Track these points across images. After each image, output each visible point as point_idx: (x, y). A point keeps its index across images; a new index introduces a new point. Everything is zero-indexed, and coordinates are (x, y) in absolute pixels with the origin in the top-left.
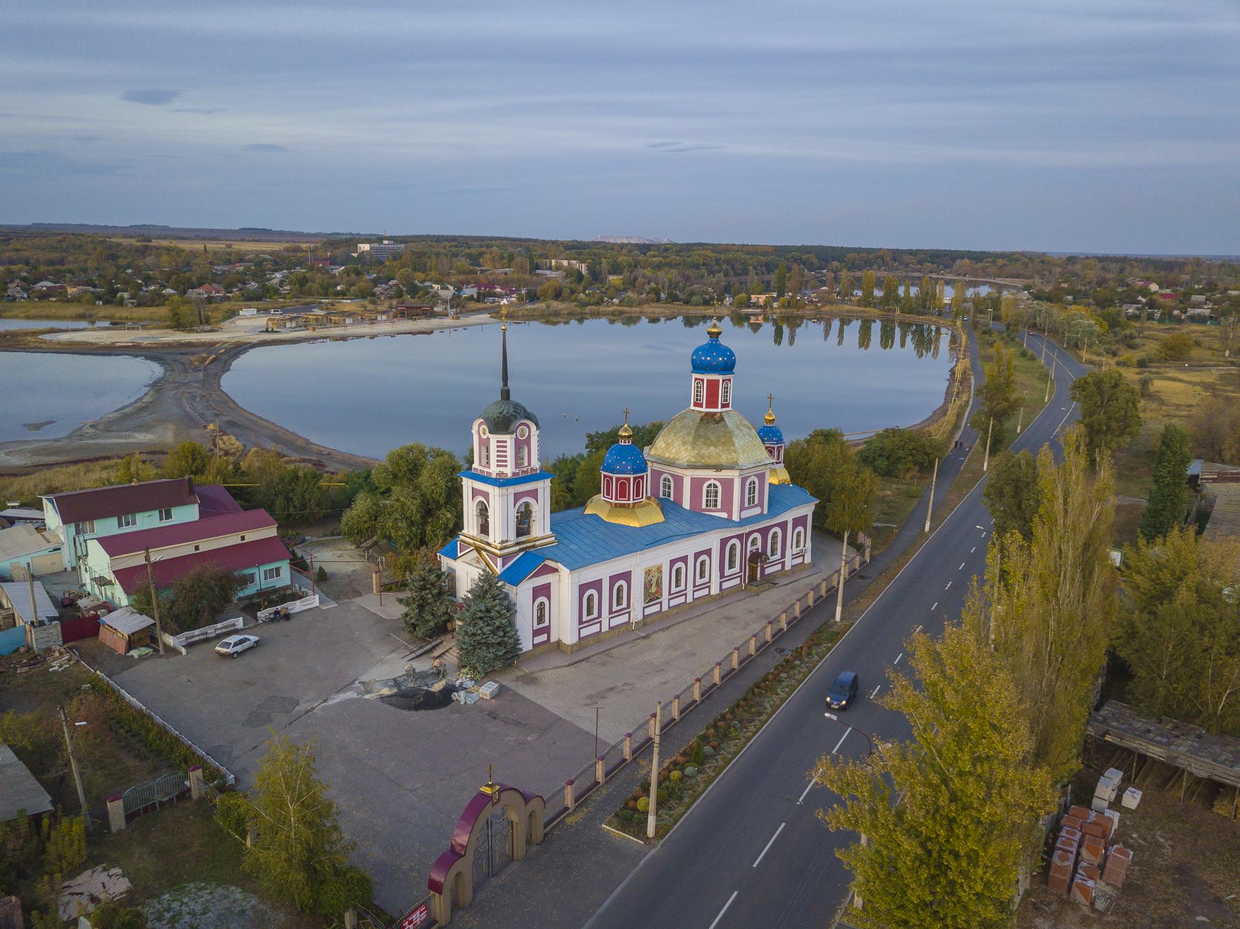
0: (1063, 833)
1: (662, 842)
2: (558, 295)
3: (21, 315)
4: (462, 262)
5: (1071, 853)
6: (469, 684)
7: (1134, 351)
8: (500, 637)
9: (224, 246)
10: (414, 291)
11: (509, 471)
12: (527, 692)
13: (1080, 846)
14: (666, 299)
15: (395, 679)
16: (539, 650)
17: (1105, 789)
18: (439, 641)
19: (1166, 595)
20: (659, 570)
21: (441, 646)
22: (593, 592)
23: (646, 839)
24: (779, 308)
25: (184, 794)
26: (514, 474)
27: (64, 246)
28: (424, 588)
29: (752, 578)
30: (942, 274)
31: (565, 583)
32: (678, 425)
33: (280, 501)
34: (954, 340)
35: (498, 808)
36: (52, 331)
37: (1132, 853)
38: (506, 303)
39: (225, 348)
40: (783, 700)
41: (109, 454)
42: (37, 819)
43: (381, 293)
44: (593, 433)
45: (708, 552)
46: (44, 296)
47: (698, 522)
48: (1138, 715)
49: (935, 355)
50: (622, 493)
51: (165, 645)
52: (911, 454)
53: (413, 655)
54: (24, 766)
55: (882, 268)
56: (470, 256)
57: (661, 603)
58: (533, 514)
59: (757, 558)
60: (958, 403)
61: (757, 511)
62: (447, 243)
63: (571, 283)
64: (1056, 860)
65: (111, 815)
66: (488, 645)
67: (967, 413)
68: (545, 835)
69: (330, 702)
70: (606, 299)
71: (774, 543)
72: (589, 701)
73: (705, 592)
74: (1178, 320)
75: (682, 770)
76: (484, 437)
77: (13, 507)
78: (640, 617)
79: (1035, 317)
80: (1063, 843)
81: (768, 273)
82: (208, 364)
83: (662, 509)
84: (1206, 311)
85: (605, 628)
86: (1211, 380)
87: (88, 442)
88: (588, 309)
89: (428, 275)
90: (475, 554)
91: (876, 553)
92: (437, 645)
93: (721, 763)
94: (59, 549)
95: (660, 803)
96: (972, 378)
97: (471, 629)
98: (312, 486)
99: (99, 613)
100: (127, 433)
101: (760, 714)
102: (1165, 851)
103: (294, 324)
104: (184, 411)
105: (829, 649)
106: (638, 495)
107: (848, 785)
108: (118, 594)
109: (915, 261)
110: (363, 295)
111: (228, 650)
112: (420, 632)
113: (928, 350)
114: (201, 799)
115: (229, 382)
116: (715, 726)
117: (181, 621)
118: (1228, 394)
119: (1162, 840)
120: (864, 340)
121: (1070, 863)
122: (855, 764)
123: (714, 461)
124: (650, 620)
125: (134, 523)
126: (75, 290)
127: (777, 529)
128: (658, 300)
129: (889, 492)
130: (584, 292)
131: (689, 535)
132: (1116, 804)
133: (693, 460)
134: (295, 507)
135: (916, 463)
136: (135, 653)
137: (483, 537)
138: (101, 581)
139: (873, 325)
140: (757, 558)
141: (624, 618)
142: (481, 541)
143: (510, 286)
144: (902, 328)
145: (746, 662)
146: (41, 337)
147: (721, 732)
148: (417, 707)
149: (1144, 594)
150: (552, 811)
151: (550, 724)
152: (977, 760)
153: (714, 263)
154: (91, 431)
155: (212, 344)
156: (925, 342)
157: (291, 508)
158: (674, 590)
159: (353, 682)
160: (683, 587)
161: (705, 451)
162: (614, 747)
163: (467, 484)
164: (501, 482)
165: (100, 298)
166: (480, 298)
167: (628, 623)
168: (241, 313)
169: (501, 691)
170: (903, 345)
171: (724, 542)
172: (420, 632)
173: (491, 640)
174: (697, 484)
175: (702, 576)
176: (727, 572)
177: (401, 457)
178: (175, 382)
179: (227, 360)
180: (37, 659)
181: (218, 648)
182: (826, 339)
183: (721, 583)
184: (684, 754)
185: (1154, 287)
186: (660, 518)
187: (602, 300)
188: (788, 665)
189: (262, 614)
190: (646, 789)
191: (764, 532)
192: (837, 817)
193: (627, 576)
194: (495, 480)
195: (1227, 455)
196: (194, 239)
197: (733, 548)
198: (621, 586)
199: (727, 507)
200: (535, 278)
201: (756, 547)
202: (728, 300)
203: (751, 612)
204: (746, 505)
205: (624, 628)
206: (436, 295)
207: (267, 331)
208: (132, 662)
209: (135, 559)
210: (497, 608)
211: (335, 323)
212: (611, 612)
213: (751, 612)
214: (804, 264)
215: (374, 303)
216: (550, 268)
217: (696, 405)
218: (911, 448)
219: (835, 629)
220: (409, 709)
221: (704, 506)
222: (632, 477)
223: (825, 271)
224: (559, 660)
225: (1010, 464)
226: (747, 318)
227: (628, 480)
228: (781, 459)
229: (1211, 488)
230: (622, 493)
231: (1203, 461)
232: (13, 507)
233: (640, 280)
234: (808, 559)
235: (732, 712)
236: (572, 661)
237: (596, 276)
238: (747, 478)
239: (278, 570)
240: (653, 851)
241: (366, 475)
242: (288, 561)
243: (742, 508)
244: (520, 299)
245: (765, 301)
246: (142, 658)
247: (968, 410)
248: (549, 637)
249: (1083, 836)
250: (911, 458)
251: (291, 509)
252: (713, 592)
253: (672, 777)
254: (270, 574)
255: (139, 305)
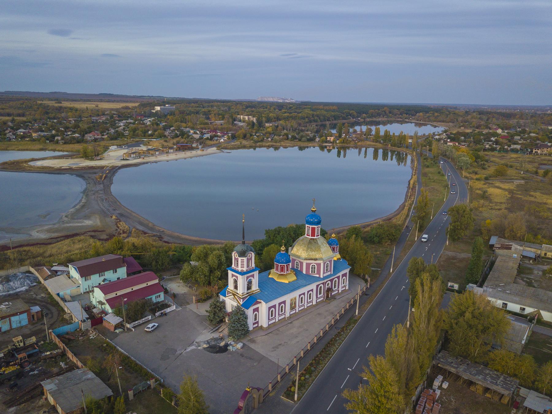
0: (421, 399)
1: (299, 402)
2: (245, 137)
3: (16, 149)
4: (202, 118)
5: (422, 405)
6: (233, 343)
7: (485, 171)
8: (243, 327)
9: (94, 106)
10: (183, 134)
11: (245, 269)
12: (252, 346)
13: (426, 402)
14: (291, 138)
15: (207, 341)
16: (255, 329)
17: (436, 383)
18: (220, 325)
19: (462, 314)
20: (295, 299)
21: (221, 327)
22: (273, 309)
23: (294, 401)
24: (339, 143)
25: (149, 387)
26: (246, 270)
27: (24, 106)
28: (215, 308)
29: (327, 297)
30: (411, 120)
31: (263, 307)
32: (301, 243)
33: (154, 263)
34: (412, 161)
35: (251, 394)
36: (33, 160)
37: (440, 405)
38: (223, 141)
39: (108, 170)
40: (337, 349)
41: (77, 232)
42: (109, 398)
43: (168, 135)
44: (268, 230)
45: (312, 290)
46: (23, 137)
47: (309, 279)
48: (450, 356)
49: (405, 165)
50: (282, 270)
51: (127, 328)
52: (388, 236)
53: (212, 331)
54: (99, 379)
55: (385, 117)
56: (205, 113)
57: (296, 310)
58: (253, 283)
59: (329, 290)
60: (410, 202)
61: (329, 273)
62: (193, 104)
63: (250, 129)
64: (417, 408)
65: (129, 395)
66: (239, 330)
67: (413, 207)
68: (264, 400)
69: (187, 350)
70: (265, 138)
71: (335, 284)
72: (273, 350)
73: (311, 304)
74: (507, 151)
75: (305, 376)
76: (236, 257)
77: (55, 266)
78: (289, 315)
79: (446, 153)
80: (420, 402)
81: (335, 120)
82: (104, 180)
83: (295, 274)
84: (518, 147)
85: (277, 320)
86: (513, 188)
87: (67, 225)
88: (258, 144)
89: (187, 124)
90: (233, 296)
91: (372, 283)
92: (220, 327)
93: (317, 373)
94: (79, 286)
95: (299, 389)
96: (417, 186)
97: (233, 325)
98: (165, 256)
99: (102, 316)
100: (81, 220)
101: (329, 354)
102: (453, 403)
103: (134, 155)
104: (100, 207)
105: (353, 327)
106: (287, 271)
107: (352, 397)
108: (108, 308)
109: (399, 113)
110: (161, 136)
111: (149, 330)
112: (214, 322)
113: (402, 162)
114: (154, 388)
115: (114, 189)
116: (315, 360)
117: (131, 318)
118: (518, 196)
119: (452, 399)
120: (376, 157)
121: (422, 410)
122: (354, 392)
123: (314, 257)
124: (292, 316)
125: (104, 275)
126: (36, 134)
127: (336, 279)
128: (288, 139)
129: (378, 253)
130: (255, 135)
131: (306, 285)
132: (440, 387)
133: (307, 257)
134: (159, 265)
135: (389, 239)
136: (117, 331)
137: (235, 290)
138: (101, 303)
139: (379, 150)
140: (329, 290)
141: (283, 316)
142: (235, 292)
143: (224, 132)
144: (391, 153)
145: (325, 333)
146: (29, 163)
147: (317, 361)
148: (217, 352)
149: (457, 313)
150: (266, 391)
151: (261, 358)
152: (385, 392)
153: (311, 116)
154: (66, 219)
155: (102, 168)
156: (401, 159)
157: (158, 265)
158: (300, 304)
159: (193, 342)
160: (303, 303)
161: (310, 253)
162: (284, 368)
163: (230, 273)
164: (242, 273)
165: (48, 139)
166: (211, 139)
167: (285, 318)
168: (110, 148)
169: (244, 345)
170: (392, 159)
171: (317, 286)
172: (214, 322)
173: (240, 328)
174: (308, 265)
175: (310, 299)
176: (319, 296)
177: (202, 252)
178: (93, 191)
179: (111, 177)
180: (85, 333)
181: (145, 329)
182: (359, 155)
183: (316, 300)
184: (305, 370)
185: (499, 131)
186: (294, 278)
187: (264, 139)
188: (338, 335)
189: (157, 314)
190: (294, 383)
191: (332, 281)
192: (349, 406)
193: (284, 302)
194: (240, 272)
195: (506, 235)
196: (79, 101)
197: (321, 287)
198: (282, 306)
199: (319, 273)
200: (234, 127)
201: (329, 286)
202: (317, 139)
203: (327, 311)
204: (325, 272)
205: (283, 320)
206: (193, 138)
207: (124, 159)
208: (117, 335)
209: (112, 295)
210: (242, 318)
211: (152, 155)
212: (279, 315)
213: (327, 311)
214: (350, 115)
215: (166, 141)
216: (240, 121)
217: (307, 235)
218: (387, 234)
219: (356, 318)
220: (214, 353)
221: (310, 273)
222: (285, 265)
223: (359, 118)
224: (262, 333)
225: (415, 263)
226: (326, 147)
227: (284, 266)
228: (338, 251)
229: (498, 251)
230: (282, 270)
231: (498, 237)
232: (55, 266)
233: (280, 127)
234: (347, 288)
235: (320, 354)
236: (266, 333)
237: (260, 124)
238: (325, 263)
239: (159, 295)
240: (297, 405)
241: (183, 248)
242: (163, 292)
243: (324, 273)
244: (229, 139)
245: (334, 140)
246: (121, 332)
247: (413, 205)
248: (258, 325)
249: (427, 399)
250: (387, 238)
251: (158, 266)
252: (314, 304)
253: (302, 379)
254: (156, 297)
255: (65, 143)
